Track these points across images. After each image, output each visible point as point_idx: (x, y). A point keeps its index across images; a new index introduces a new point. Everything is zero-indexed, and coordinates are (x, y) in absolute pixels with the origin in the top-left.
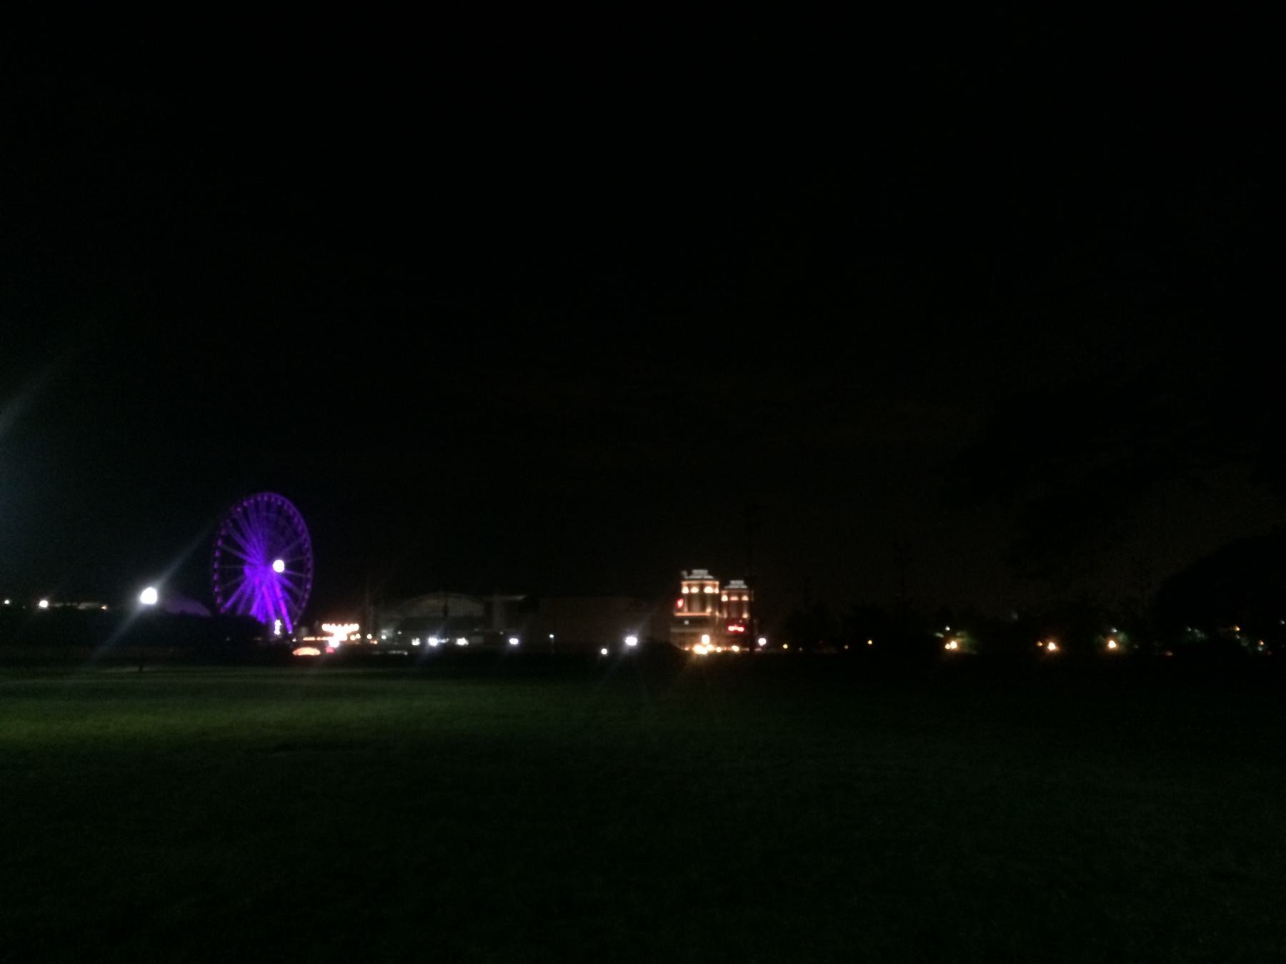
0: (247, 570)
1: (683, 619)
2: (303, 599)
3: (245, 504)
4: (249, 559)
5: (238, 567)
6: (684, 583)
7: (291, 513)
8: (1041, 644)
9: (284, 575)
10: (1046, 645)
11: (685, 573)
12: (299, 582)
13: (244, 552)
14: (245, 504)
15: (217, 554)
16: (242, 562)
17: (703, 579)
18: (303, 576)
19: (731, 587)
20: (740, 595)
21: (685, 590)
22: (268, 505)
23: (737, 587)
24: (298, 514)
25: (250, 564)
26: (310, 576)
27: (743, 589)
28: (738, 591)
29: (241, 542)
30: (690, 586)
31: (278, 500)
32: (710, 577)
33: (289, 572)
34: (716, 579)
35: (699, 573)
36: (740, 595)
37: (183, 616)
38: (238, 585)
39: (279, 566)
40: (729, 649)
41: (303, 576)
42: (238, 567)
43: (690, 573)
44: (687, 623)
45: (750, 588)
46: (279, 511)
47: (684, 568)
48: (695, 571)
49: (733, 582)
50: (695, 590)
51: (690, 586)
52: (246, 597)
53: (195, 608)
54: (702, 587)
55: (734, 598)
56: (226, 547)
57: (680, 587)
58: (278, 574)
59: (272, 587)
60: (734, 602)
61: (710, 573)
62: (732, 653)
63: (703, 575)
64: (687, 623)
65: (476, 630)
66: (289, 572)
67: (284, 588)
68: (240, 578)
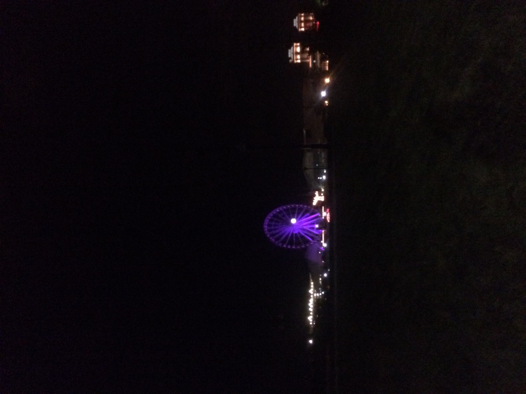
1: (313, 63)
2: (307, 208)
3: (269, 236)
6: (295, 61)
7: (272, 215)
13: (289, 233)
14: (269, 236)
16: (292, 234)
18: (297, 209)
19: (297, 27)
20: (301, 22)
21: (299, 61)
22: (269, 225)
23: (297, 23)
24: (272, 212)
25: (293, 230)
26: (297, 206)
28: (299, 23)
29: (284, 236)
30: (297, 59)
31: (267, 222)
33: (296, 217)
34: (292, 45)
35: (290, 55)
36: (301, 22)
37: (332, 76)
38: (302, 237)
39: (293, 221)
41: (297, 209)
42: (296, 215)
43: (290, 58)
44: (315, 61)
45: (297, 15)
47: (288, 62)
48: (289, 56)
49: (295, 25)
50: (299, 57)
51: (297, 59)
53: (327, 88)
54: (297, 53)
55: (303, 24)
57: (298, 63)
58: (297, 221)
59: (301, 223)
60: (304, 24)
61: (290, 48)
62: (329, 63)
64: (315, 61)
65: (319, 153)
66: (296, 217)
67: (300, 218)
68: (299, 236)
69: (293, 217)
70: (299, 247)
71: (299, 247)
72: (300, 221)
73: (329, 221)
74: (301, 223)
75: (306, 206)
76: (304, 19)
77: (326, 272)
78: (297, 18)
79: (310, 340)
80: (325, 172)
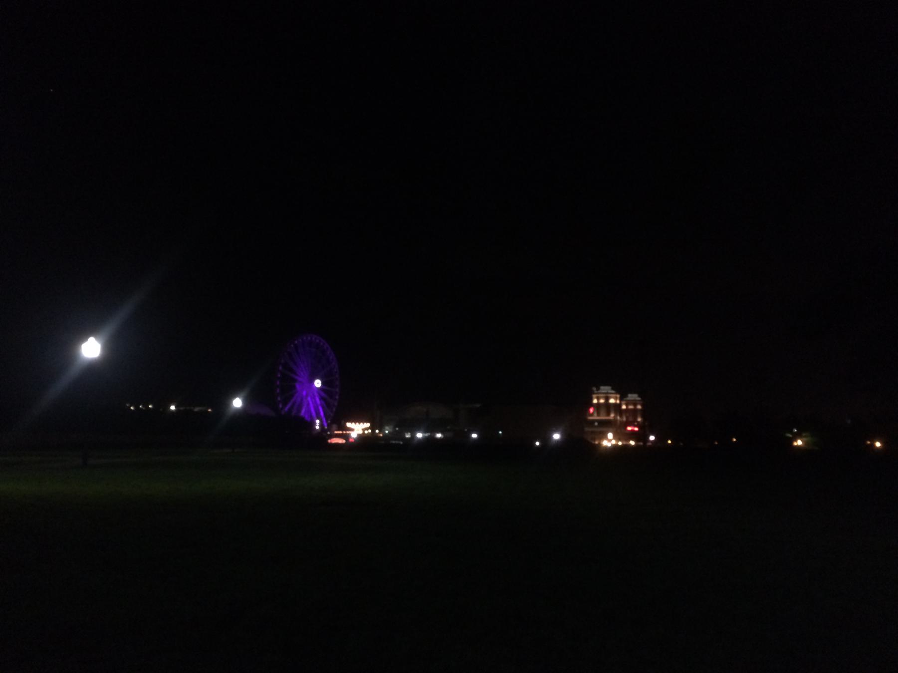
0: (298, 387)
6: (594, 396)
8: (869, 442)
11: (594, 389)
17: (607, 393)
19: (628, 399)
20: (635, 405)
21: (595, 401)
30: (598, 399)
32: (613, 392)
35: (605, 389)
36: (635, 405)
43: (598, 389)
44: (596, 424)
48: (602, 388)
54: (607, 399)
55: (631, 407)
61: (613, 389)
64: (596, 424)
65: (448, 427)
69: (323, 383)
70: (278, 391)
71: (278, 391)
72: (316, 394)
73: (329, 441)
74: (313, 397)
75: (336, 404)
76: (639, 409)
77: (873, 445)
78: (639, 399)
79: (172, 410)
80: (869, 442)
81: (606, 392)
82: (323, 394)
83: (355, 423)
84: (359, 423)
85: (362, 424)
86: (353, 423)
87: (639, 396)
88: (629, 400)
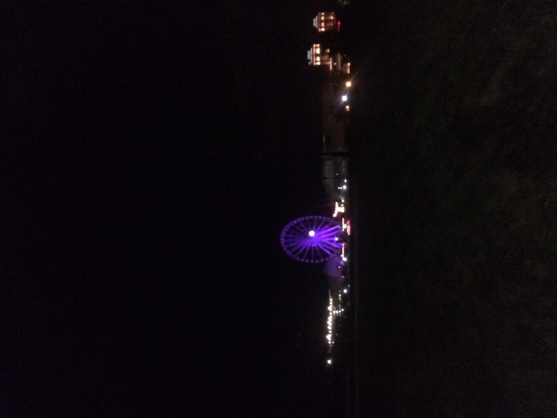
0: (315, 245)
4: (310, 245)
5: (312, 249)
6: (315, 64)
8: (347, 107)
9: (315, 231)
10: (346, 104)
11: (310, 63)
12: (319, 221)
13: (307, 247)
15: (307, 261)
16: (311, 247)
17: (313, 55)
18: (316, 220)
19: (317, 27)
20: (321, 21)
21: (319, 63)
22: (286, 238)
23: (317, 23)
25: (311, 244)
27: (318, 19)
30: (316, 62)
31: (283, 234)
32: (311, 49)
35: (309, 56)
36: (321, 21)
38: (321, 251)
39: (312, 233)
40: (349, 67)
41: (316, 220)
43: (310, 60)
44: (335, 64)
46: (288, 233)
47: (307, 64)
48: (309, 58)
49: (314, 25)
50: (318, 59)
51: (316, 62)
52: (325, 246)
54: (317, 55)
55: (323, 24)
56: (305, 257)
58: (315, 233)
61: (309, 50)
62: (350, 65)
63: (316, 21)
64: (335, 64)
65: (339, 161)
68: (318, 249)
70: (317, 261)
71: (317, 261)
77: (346, 288)
78: (317, 17)
80: (345, 181)
81: (312, 56)
82: (319, 228)
83: (335, 212)
84: (335, 209)
85: (336, 208)
86: (335, 211)
87: (315, 17)
88: (318, 26)
